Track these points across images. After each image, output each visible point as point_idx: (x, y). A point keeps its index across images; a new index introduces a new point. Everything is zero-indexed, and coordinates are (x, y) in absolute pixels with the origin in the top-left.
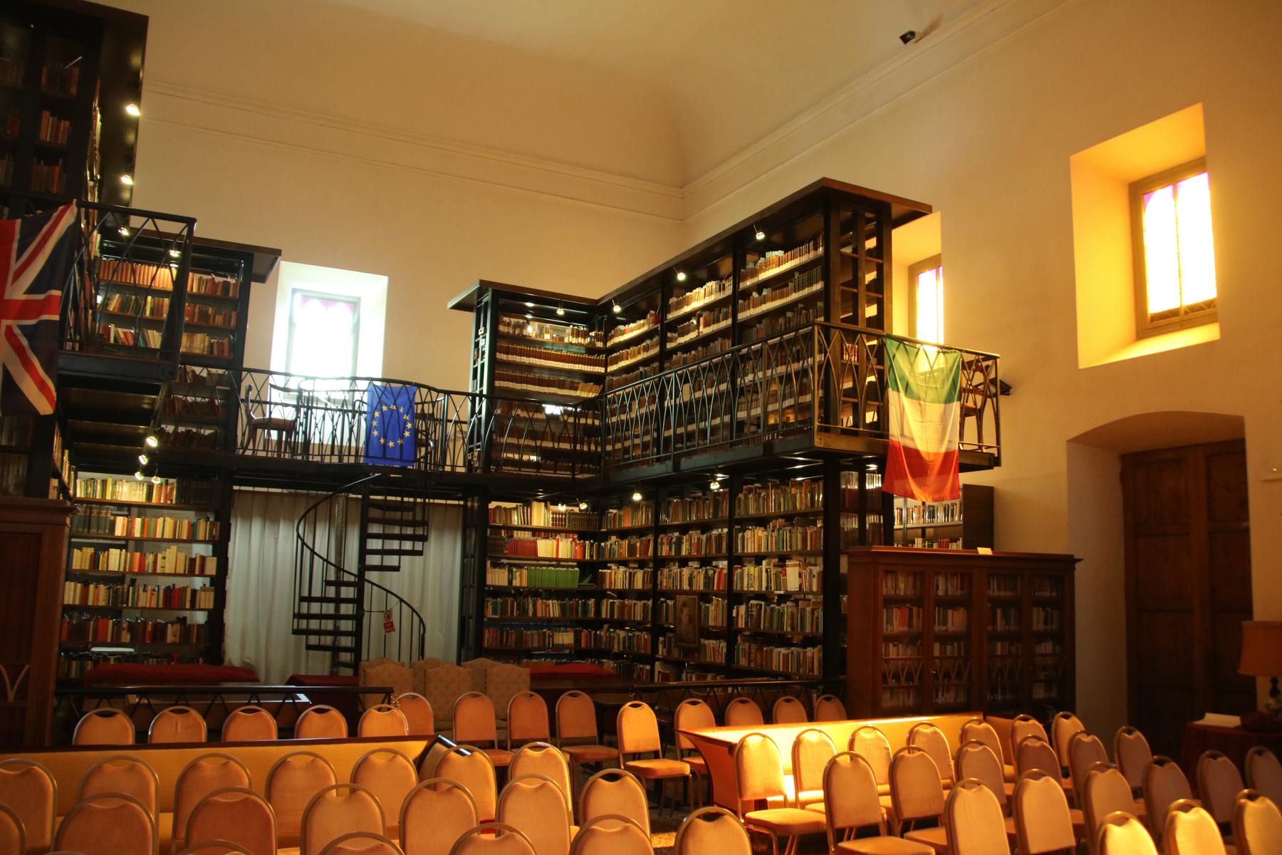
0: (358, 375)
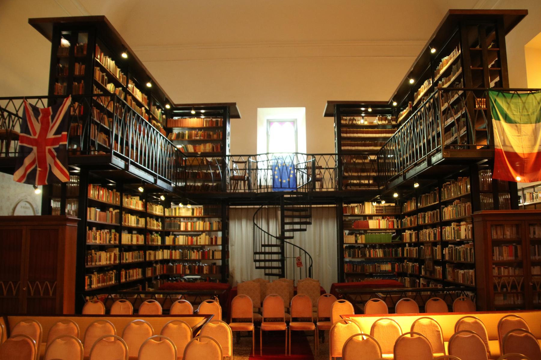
0: (299, 152)
